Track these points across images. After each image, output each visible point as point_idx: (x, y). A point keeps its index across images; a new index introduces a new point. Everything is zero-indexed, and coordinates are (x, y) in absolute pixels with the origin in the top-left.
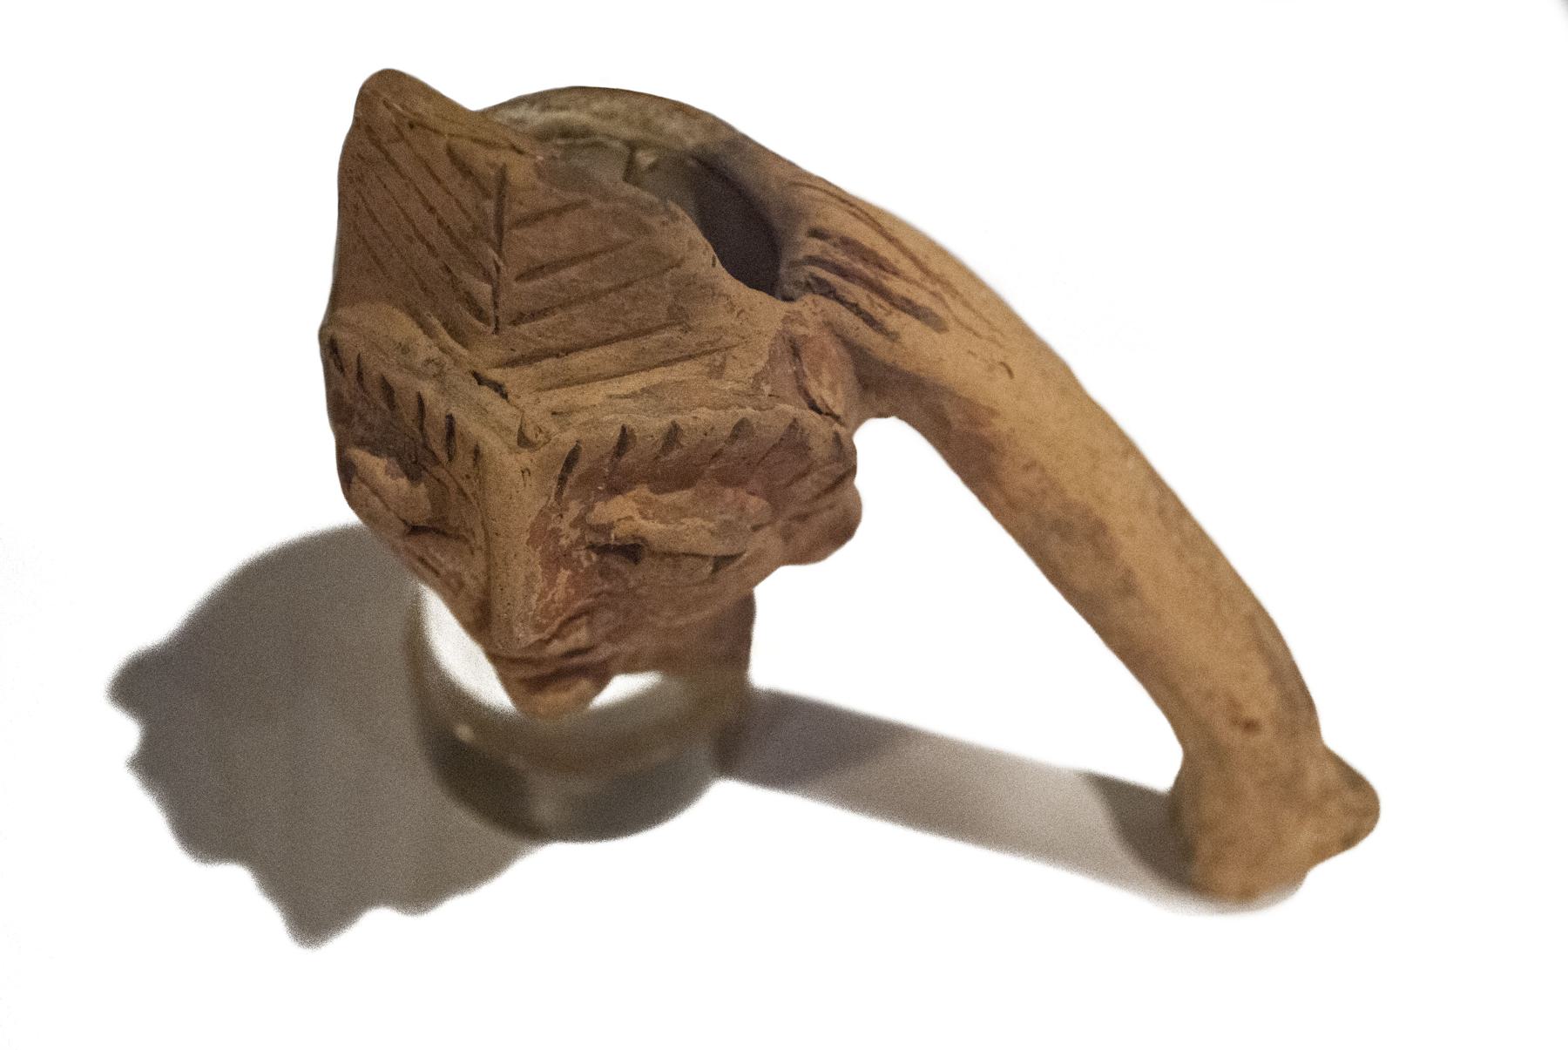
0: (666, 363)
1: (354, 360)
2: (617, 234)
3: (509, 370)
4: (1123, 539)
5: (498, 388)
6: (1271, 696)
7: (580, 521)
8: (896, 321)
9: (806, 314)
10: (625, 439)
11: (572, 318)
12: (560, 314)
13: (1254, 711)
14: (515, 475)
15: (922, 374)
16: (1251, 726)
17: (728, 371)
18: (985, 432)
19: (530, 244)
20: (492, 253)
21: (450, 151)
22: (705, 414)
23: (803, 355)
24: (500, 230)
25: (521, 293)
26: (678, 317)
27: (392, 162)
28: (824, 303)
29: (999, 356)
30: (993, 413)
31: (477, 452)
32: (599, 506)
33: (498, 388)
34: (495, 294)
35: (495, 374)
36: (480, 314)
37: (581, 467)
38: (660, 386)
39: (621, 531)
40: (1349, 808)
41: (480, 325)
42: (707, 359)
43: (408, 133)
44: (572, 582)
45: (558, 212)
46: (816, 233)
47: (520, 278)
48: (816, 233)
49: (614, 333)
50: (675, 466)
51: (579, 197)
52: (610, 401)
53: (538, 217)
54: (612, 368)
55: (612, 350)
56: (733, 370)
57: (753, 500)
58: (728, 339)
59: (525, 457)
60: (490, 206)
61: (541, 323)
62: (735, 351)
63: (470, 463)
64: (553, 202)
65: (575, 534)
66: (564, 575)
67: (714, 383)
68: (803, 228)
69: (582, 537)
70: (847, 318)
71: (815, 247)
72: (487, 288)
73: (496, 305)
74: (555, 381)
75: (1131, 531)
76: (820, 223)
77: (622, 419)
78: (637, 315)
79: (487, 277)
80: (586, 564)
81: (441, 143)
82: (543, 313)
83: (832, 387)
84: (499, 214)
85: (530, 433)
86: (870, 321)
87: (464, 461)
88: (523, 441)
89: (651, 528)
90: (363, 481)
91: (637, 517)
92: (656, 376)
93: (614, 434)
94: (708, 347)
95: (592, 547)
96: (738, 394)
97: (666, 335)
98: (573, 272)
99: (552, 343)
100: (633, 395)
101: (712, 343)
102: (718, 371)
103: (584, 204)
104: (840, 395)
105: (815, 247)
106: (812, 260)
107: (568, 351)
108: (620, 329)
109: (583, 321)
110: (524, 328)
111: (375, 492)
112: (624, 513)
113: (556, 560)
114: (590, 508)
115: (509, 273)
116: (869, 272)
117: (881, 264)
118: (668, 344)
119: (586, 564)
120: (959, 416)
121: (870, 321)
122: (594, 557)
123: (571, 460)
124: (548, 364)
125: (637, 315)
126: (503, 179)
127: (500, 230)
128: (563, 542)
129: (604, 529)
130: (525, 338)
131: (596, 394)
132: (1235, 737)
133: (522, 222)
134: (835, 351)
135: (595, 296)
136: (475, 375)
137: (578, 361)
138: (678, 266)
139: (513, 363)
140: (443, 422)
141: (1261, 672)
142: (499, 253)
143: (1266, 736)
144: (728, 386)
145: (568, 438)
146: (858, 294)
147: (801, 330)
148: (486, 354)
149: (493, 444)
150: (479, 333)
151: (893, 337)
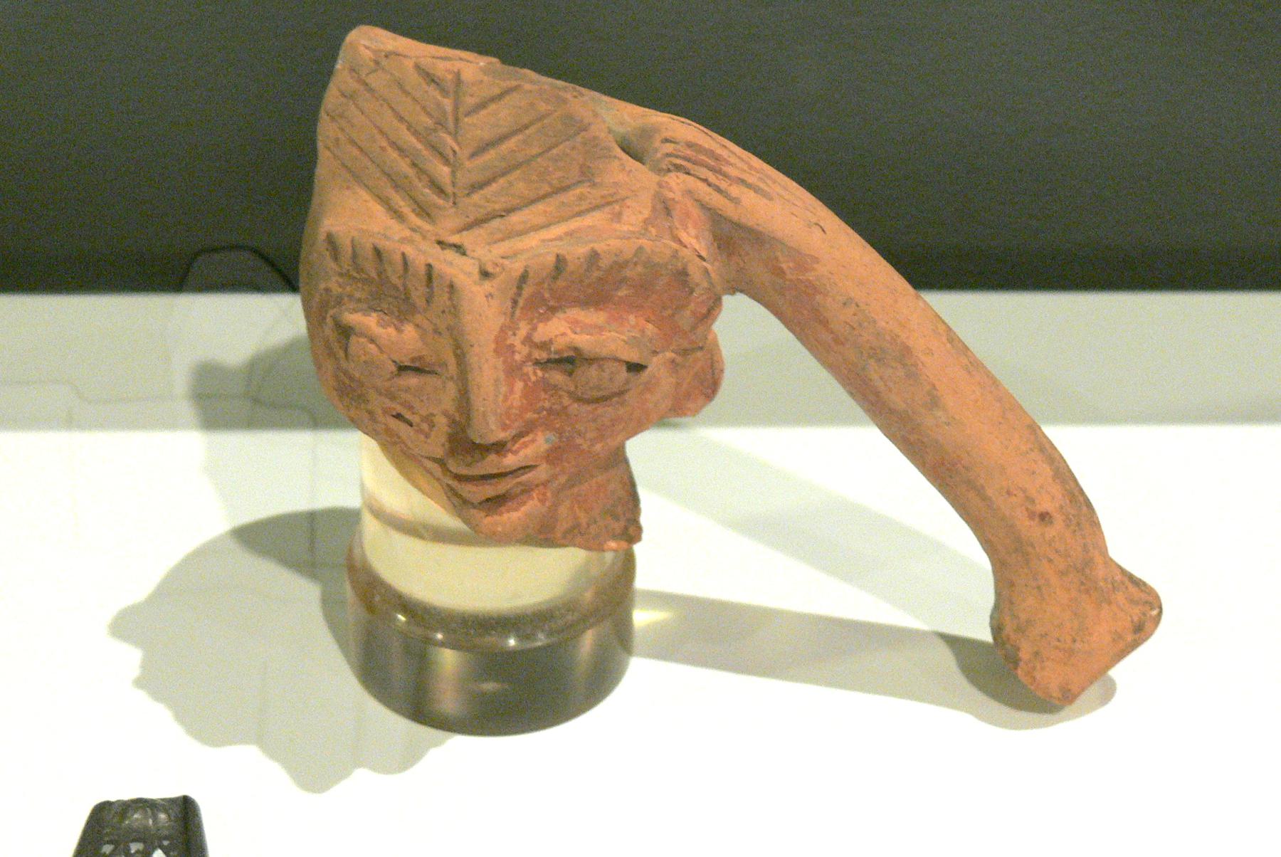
0: (579, 214)
1: (348, 242)
2: (543, 107)
3: (465, 233)
4: (923, 358)
5: (459, 248)
6: (1056, 490)
7: (528, 340)
8: (735, 190)
9: (673, 184)
10: (560, 262)
11: (511, 184)
12: (502, 181)
13: (1045, 505)
14: (480, 299)
15: (760, 229)
16: (1044, 517)
17: (625, 218)
18: (810, 276)
19: (479, 126)
20: (449, 140)
21: (417, 67)
22: (615, 243)
23: (674, 213)
24: (457, 120)
25: (473, 168)
26: (587, 176)
27: (371, 90)
28: (683, 176)
29: (814, 220)
30: (816, 260)
31: (452, 286)
32: (541, 326)
33: (459, 248)
34: (453, 173)
35: (455, 239)
36: (440, 191)
37: (527, 291)
38: (579, 230)
39: (560, 343)
40: (1138, 612)
41: (441, 202)
42: (607, 209)
43: (384, 62)
44: (525, 394)
45: (501, 96)
46: (667, 140)
47: (473, 155)
48: (667, 140)
49: (542, 192)
50: (595, 284)
51: (514, 83)
52: (540, 241)
53: (483, 105)
54: (541, 220)
55: (540, 207)
56: (627, 214)
57: (650, 326)
58: (623, 193)
59: (488, 286)
60: (447, 104)
61: (488, 191)
62: (628, 202)
63: (446, 296)
64: (497, 91)
65: (525, 350)
66: (519, 385)
67: (617, 226)
68: (658, 138)
69: (530, 355)
70: (702, 187)
71: (669, 148)
72: (446, 170)
73: (454, 184)
74: (500, 236)
75: (930, 352)
76: (668, 134)
77: (556, 250)
78: (560, 174)
79: (447, 162)
80: (533, 378)
81: (409, 64)
82: (487, 183)
83: (697, 237)
84: (456, 108)
85: (490, 269)
86: (718, 190)
87: (442, 299)
88: (485, 274)
89: (583, 341)
90: (362, 334)
91: (569, 332)
92: (574, 224)
93: (551, 259)
94: (610, 199)
95: (537, 363)
96: (633, 232)
97: (578, 191)
98: (512, 143)
99: (497, 207)
100: (560, 238)
101: (612, 195)
102: (618, 217)
103: (516, 88)
104: (703, 244)
105: (669, 148)
106: (668, 155)
107: (510, 211)
108: (547, 188)
109: (519, 185)
110: (476, 197)
111: (372, 341)
112: (560, 330)
113: (513, 371)
114: (534, 329)
115: (463, 154)
116: (712, 162)
117: (717, 158)
118: (581, 198)
119: (533, 378)
120: (791, 265)
121: (718, 190)
122: (540, 373)
123: (524, 278)
124: (496, 223)
125: (560, 174)
126: (458, 81)
127: (457, 120)
128: (517, 357)
129: (544, 346)
130: (475, 205)
131: (532, 241)
132: (1030, 529)
133: (468, 114)
134: (696, 212)
135: (528, 161)
136: (440, 243)
137: (515, 218)
138: (585, 130)
139: (468, 227)
140: (422, 271)
141: (1046, 470)
142: (456, 140)
143: (1056, 528)
144: (625, 228)
145: (517, 267)
146: (704, 173)
147: (671, 195)
148: (447, 225)
149: (461, 280)
150: (439, 208)
151: (736, 201)
